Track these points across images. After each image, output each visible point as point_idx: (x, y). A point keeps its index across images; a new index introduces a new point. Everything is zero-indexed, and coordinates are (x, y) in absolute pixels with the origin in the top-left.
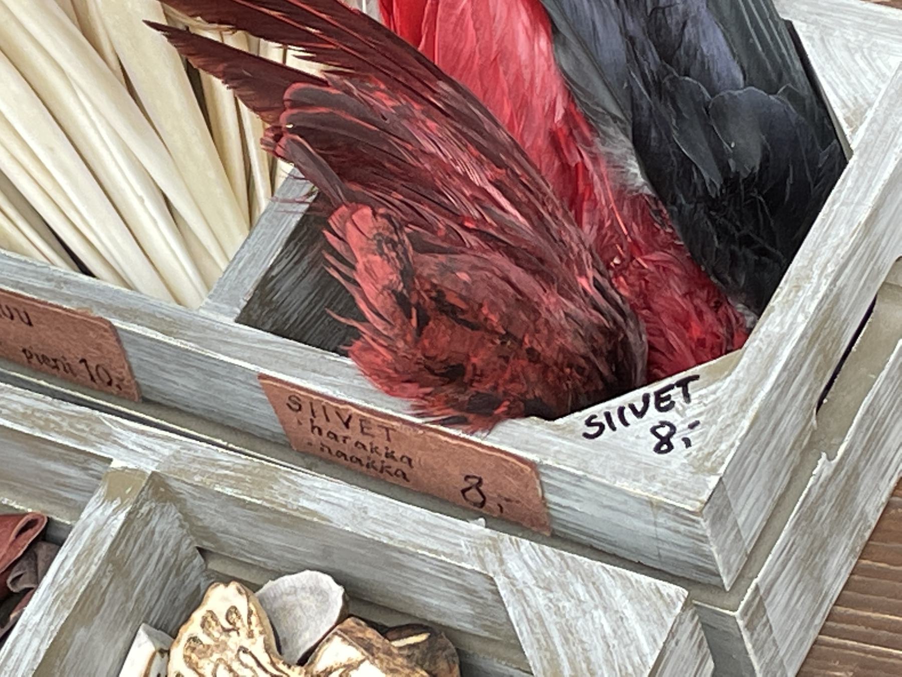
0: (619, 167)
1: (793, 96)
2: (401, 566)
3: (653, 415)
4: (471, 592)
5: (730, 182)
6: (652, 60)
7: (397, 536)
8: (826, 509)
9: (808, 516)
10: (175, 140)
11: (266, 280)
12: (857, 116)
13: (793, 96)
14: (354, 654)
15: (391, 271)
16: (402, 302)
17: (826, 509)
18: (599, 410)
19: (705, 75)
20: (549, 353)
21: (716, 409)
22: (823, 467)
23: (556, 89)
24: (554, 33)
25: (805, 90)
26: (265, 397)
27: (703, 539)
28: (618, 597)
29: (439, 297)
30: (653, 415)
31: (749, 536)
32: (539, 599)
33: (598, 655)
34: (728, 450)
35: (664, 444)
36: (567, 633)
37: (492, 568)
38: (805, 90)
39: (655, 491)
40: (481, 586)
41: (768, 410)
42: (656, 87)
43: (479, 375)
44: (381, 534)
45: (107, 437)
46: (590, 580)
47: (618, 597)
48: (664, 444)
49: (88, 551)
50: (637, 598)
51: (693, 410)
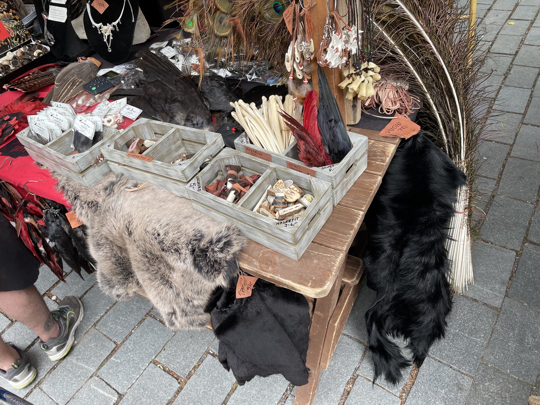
0: (326, 150)
1: (347, 142)
2: (300, 180)
3: (329, 168)
4: (307, 183)
5: (339, 151)
6: (332, 137)
7: (301, 176)
8: (345, 185)
9: (343, 184)
10: (279, 141)
11: (288, 153)
12: (354, 144)
13: (347, 142)
14: (294, 187)
15: (216, 353)
16: (305, 150)
17: (345, 185)
18: (323, 167)
19: (338, 139)
20: (319, 161)
21: (336, 168)
22: (345, 180)
23: (320, 141)
24: (321, 135)
25: (349, 141)
26: (211, 328)
27: (333, 181)
28: (324, 183)
29: (309, 152)
30: (329, 168)
31: (338, 182)
32: (315, 183)
33: (321, 188)
34: (337, 172)
35: (330, 170)
36: (318, 186)
37: (310, 179)
38: (349, 141)
39: (329, 175)
40: (309, 181)
41: (341, 169)
42: (333, 141)
43: (311, 161)
44: (299, 175)
45: (270, 164)
46: (321, 181)
47: (324, 183)
48: (330, 170)
49: (267, 174)
50: (326, 183)
51: (334, 168)
